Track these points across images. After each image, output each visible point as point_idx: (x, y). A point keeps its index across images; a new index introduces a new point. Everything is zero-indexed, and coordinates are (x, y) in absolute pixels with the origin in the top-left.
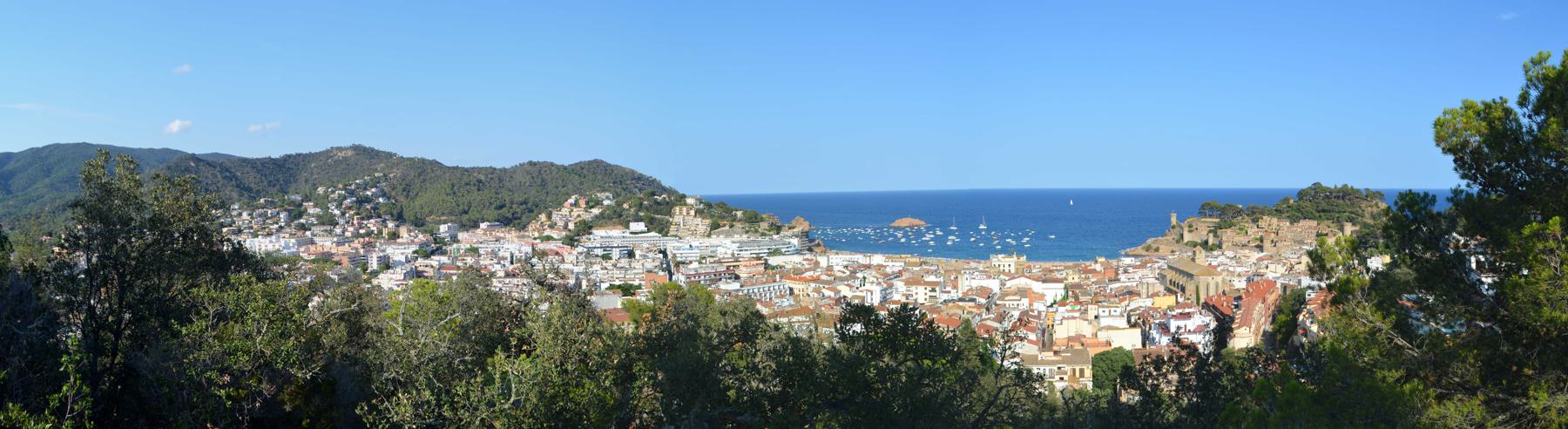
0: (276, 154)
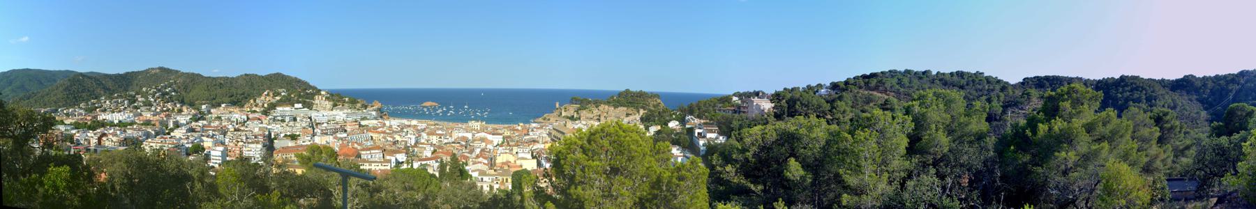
0: (122, 72)
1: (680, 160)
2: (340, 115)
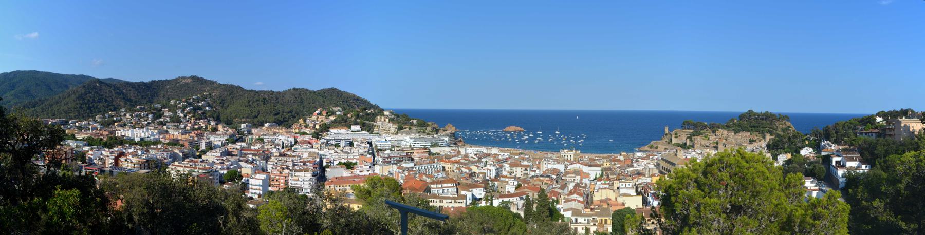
1: (814, 194)
2: (407, 140)
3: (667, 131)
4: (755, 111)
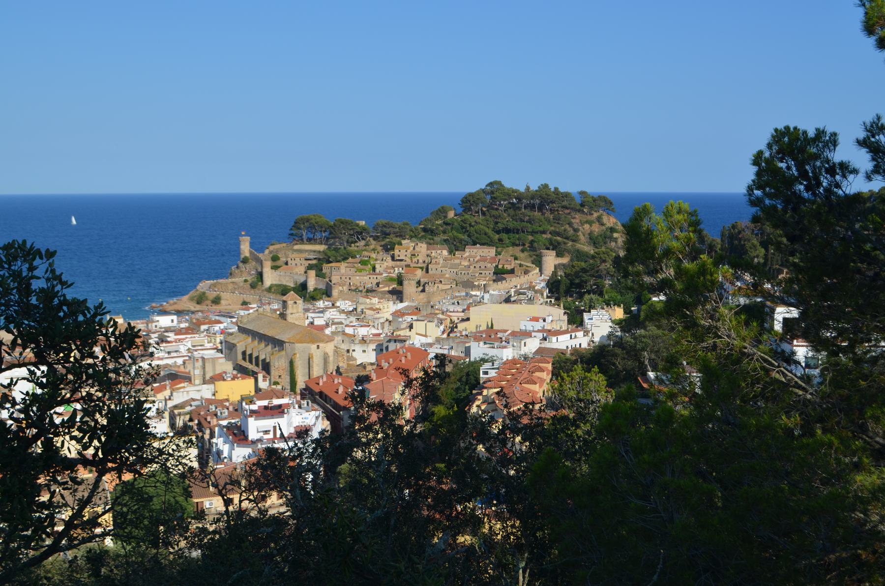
3: (245, 249)
4: (508, 184)
